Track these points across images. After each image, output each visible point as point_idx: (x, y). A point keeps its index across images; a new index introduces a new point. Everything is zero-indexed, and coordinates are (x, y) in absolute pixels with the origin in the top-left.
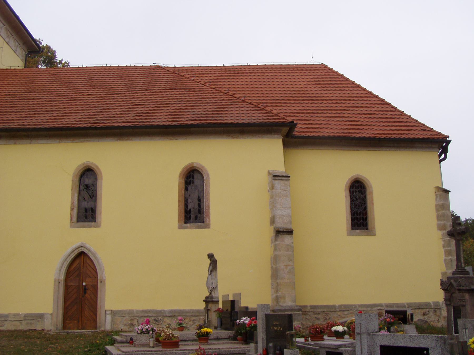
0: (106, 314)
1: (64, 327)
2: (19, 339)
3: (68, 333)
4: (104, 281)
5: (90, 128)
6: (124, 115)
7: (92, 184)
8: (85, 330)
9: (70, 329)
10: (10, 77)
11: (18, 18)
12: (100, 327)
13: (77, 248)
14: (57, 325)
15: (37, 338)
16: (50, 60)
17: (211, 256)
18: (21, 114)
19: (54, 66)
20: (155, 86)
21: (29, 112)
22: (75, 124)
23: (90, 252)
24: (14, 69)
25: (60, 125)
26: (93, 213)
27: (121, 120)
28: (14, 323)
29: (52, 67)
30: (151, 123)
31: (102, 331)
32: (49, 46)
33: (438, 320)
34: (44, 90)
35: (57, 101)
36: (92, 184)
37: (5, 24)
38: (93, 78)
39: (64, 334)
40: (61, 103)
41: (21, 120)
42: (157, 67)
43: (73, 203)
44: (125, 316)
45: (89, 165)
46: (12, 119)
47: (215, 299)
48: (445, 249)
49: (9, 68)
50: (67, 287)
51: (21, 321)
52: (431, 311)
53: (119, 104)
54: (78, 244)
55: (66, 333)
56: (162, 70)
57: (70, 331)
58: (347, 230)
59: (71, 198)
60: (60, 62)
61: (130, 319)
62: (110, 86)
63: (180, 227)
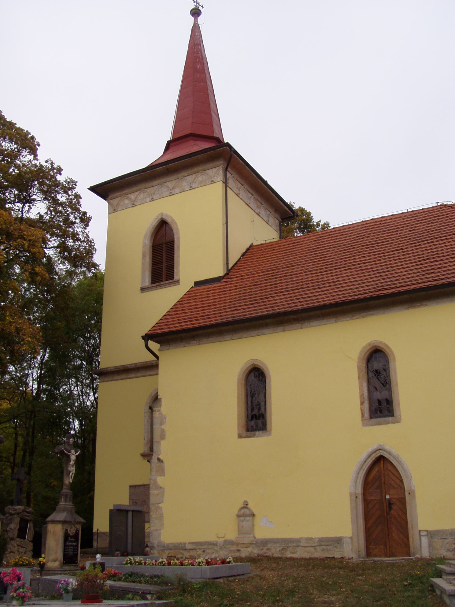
0: (420, 536)
1: (368, 554)
2: (317, 569)
3: (375, 562)
4: (414, 492)
5: (372, 298)
6: (412, 275)
7: (384, 369)
8: (396, 557)
9: (375, 556)
10: (267, 253)
11: (265, 183)
12: (414, 554)
13: (374, 451)
14: (359, 552)
15: (339, 568)
16: (305, 225)
18: (286, 295)
19: (312, 230)
20: (445, 231)
21: (294, 290)
22: (352, 296)
23: (391, 455)
24: (270, 243)
25: (334, 301)
26: (389, 405)
27: (409, 281)
28: (308, 549)
29: (310, 232)
30: (448, 280)
31: (419, 560)
32: (302, 208)
34: (307, 261)
35: (325, 271)
36: (384, 369)
37: (253, 193)
38: (364, 235)
39: (370, 563)
40: (330, 273)
41: (287, 301)
42: (441, 207)
43: (362, 395)
44: (446, 538)
45: (376, 344)
46: (277, 301)
49: (264, 242)
50: (366, 502)
51: (314, 546)
53: (402, 262)
54: (375, 446)
55: (372, 562)
56: (449, 209)
57: (376, 559)
59: (359, 388)
60: (318, 224)
62: (387, 241)
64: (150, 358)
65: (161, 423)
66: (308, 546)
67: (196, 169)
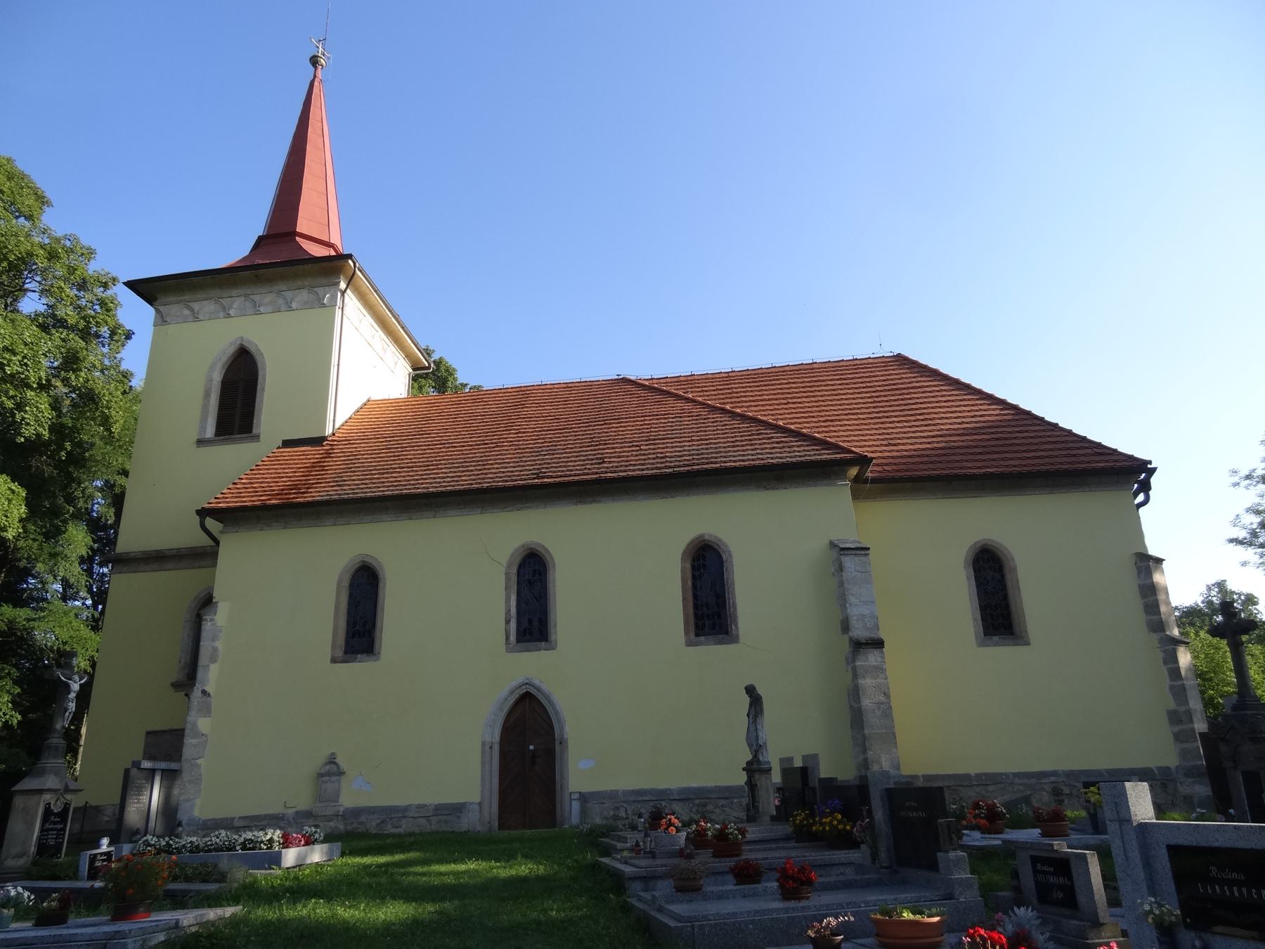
0: (571, 800)
1: (501, 827)
17: (750, 690)
33: (1173, 801)
47: (764, 766)
48: (1168, 666)
52: (1156, 785)
54: (521, 680)
58: (976, 637)
61: (613, 807)
63: (689, 644)
64: (206, 541)
65: (214, 639)
66: (420, 817)
67: (300, 283)
